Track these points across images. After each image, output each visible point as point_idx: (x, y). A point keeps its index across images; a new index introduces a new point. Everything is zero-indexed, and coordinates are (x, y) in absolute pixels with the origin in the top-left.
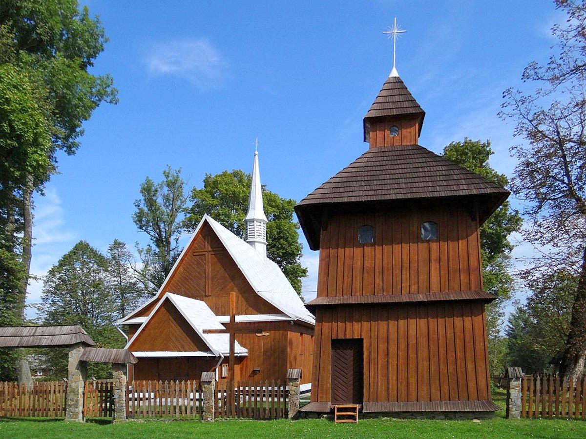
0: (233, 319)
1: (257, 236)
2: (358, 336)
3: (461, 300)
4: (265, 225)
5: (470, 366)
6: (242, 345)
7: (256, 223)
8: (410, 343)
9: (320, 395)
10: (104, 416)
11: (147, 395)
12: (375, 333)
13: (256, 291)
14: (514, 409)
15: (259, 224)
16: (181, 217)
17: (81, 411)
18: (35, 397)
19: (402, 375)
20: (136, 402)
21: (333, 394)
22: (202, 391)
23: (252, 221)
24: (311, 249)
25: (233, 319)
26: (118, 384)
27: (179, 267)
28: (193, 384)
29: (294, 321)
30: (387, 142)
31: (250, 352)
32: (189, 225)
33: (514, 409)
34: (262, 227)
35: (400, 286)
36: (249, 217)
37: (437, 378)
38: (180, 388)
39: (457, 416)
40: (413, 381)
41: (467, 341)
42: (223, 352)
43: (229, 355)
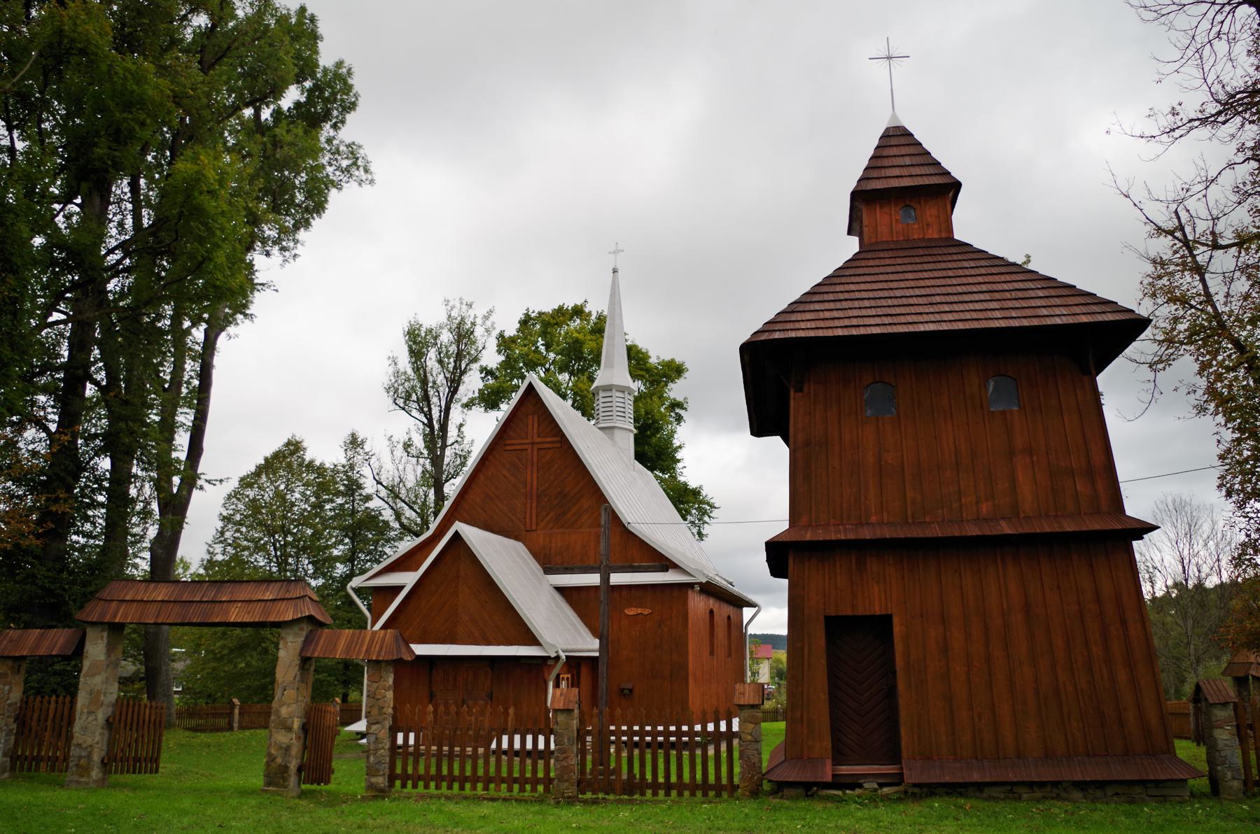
1: (618, 418)
10: (27, 771)
13: (624, 522)
14: (1229, 775)
15: (621, 395)
16: (473, 383)
18: (632, 752)
22: (551, 732)
23: (608, 388)
24: (752, 434)
29: (700, 584)
30: (897, 232)
32: (490, 399)
33: (1229, 775)
39: (1110, 791)
42: (565, 647)
43: (597, 654)
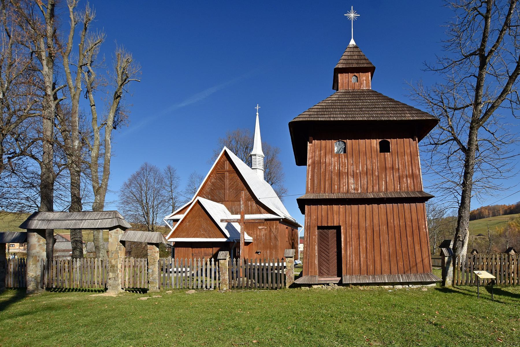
0: (243, 217)
2: (337, 224)
3: (409, 197)
4: (263, 159)
5: (417, 247)
6: (249, 234)
7: (257, 157)
8: (375, 229)
9: (310, 270)
11: (184, 269)
12: (349, 221)
17: (120, 283)
19: (370, 256)
20: (180, 274)
21: (320, 269)
23: (255, 155)
25: (243, 217)
26: (152, 261)
27: (207, 182)
28: (212, 261)
29: (282, 219)
31: (254, 239)
34: (261, 160)
35: (366, 186)
36: (252, 153)
37: (395, 256)
38: (197, 264)
40: (378, 259)
41: (414, 229)
42: (237, 239)
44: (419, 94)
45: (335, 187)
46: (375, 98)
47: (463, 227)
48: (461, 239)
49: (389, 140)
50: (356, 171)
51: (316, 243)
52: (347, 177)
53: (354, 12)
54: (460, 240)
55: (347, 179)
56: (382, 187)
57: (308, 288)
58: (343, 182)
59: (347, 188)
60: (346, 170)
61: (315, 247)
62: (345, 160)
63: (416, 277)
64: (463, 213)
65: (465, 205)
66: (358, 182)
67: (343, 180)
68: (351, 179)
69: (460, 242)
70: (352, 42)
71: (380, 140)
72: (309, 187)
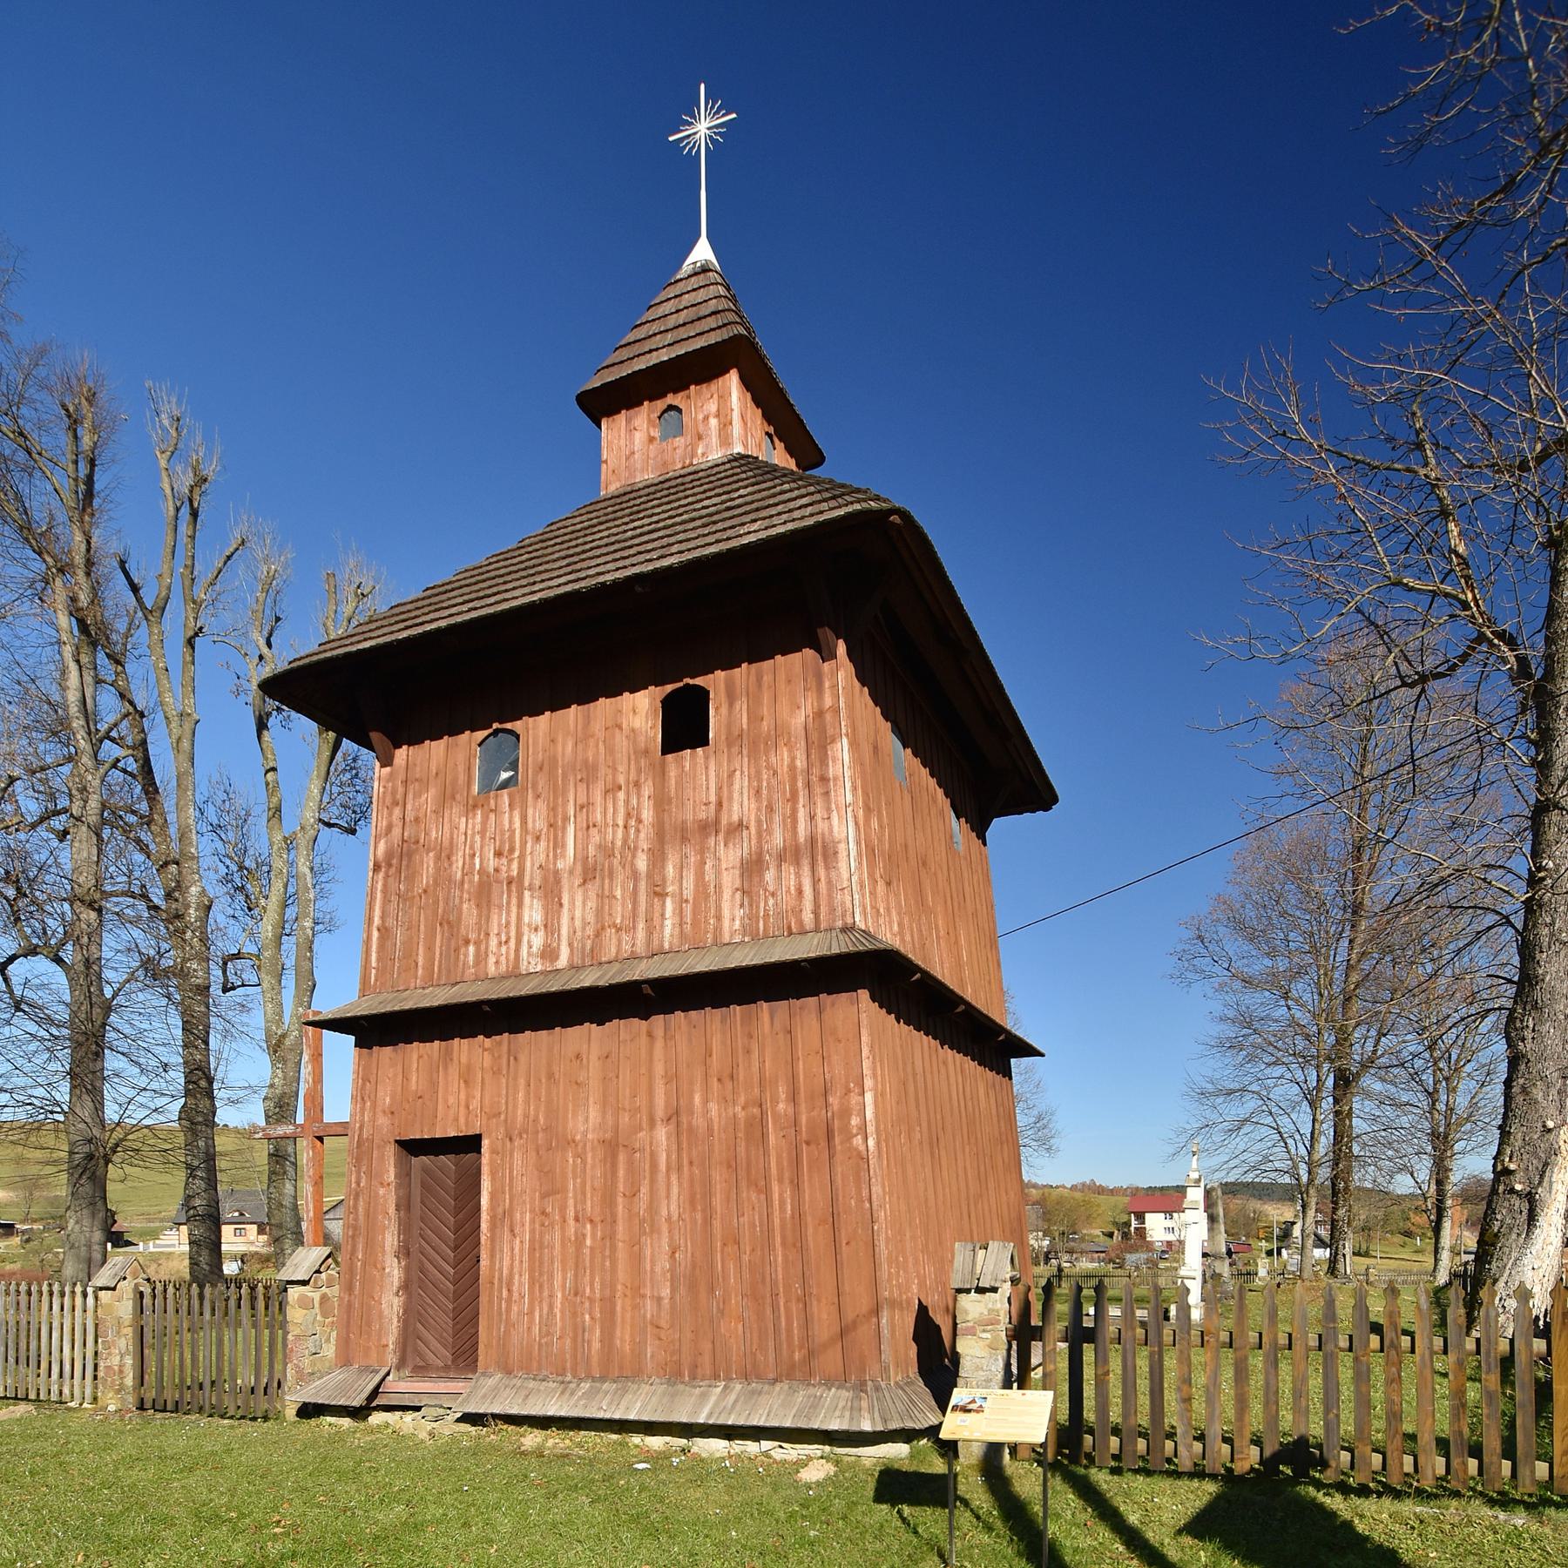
44: (1284, 434)
45: (466, 955)
46: (786, 487)
47: (1532, 1116)
48: (1518, 1187)
49: (699, 681)
50: (555, 864)
51: (390, 1220)
52: (514, 901)
53: (712, 108)
54: (1512, 1191)
55: (514, 909)
56: (662, 926)
57: (346, 1422)
58: (500, 925)
59: (512, 956)
60: (515, 866)
61: (384, 1238)
62: (511, 822)
63: (855, 1410)
64: (1528, 1034)
65: (1537, 994)
66: (559, 918)
67: (500, 916)
68: (531, 907)
69: (1516, 1201)
70: (703, 252)
71: (669, 688)
72: (374, 965)
